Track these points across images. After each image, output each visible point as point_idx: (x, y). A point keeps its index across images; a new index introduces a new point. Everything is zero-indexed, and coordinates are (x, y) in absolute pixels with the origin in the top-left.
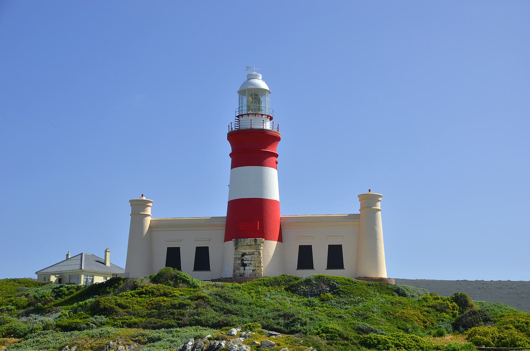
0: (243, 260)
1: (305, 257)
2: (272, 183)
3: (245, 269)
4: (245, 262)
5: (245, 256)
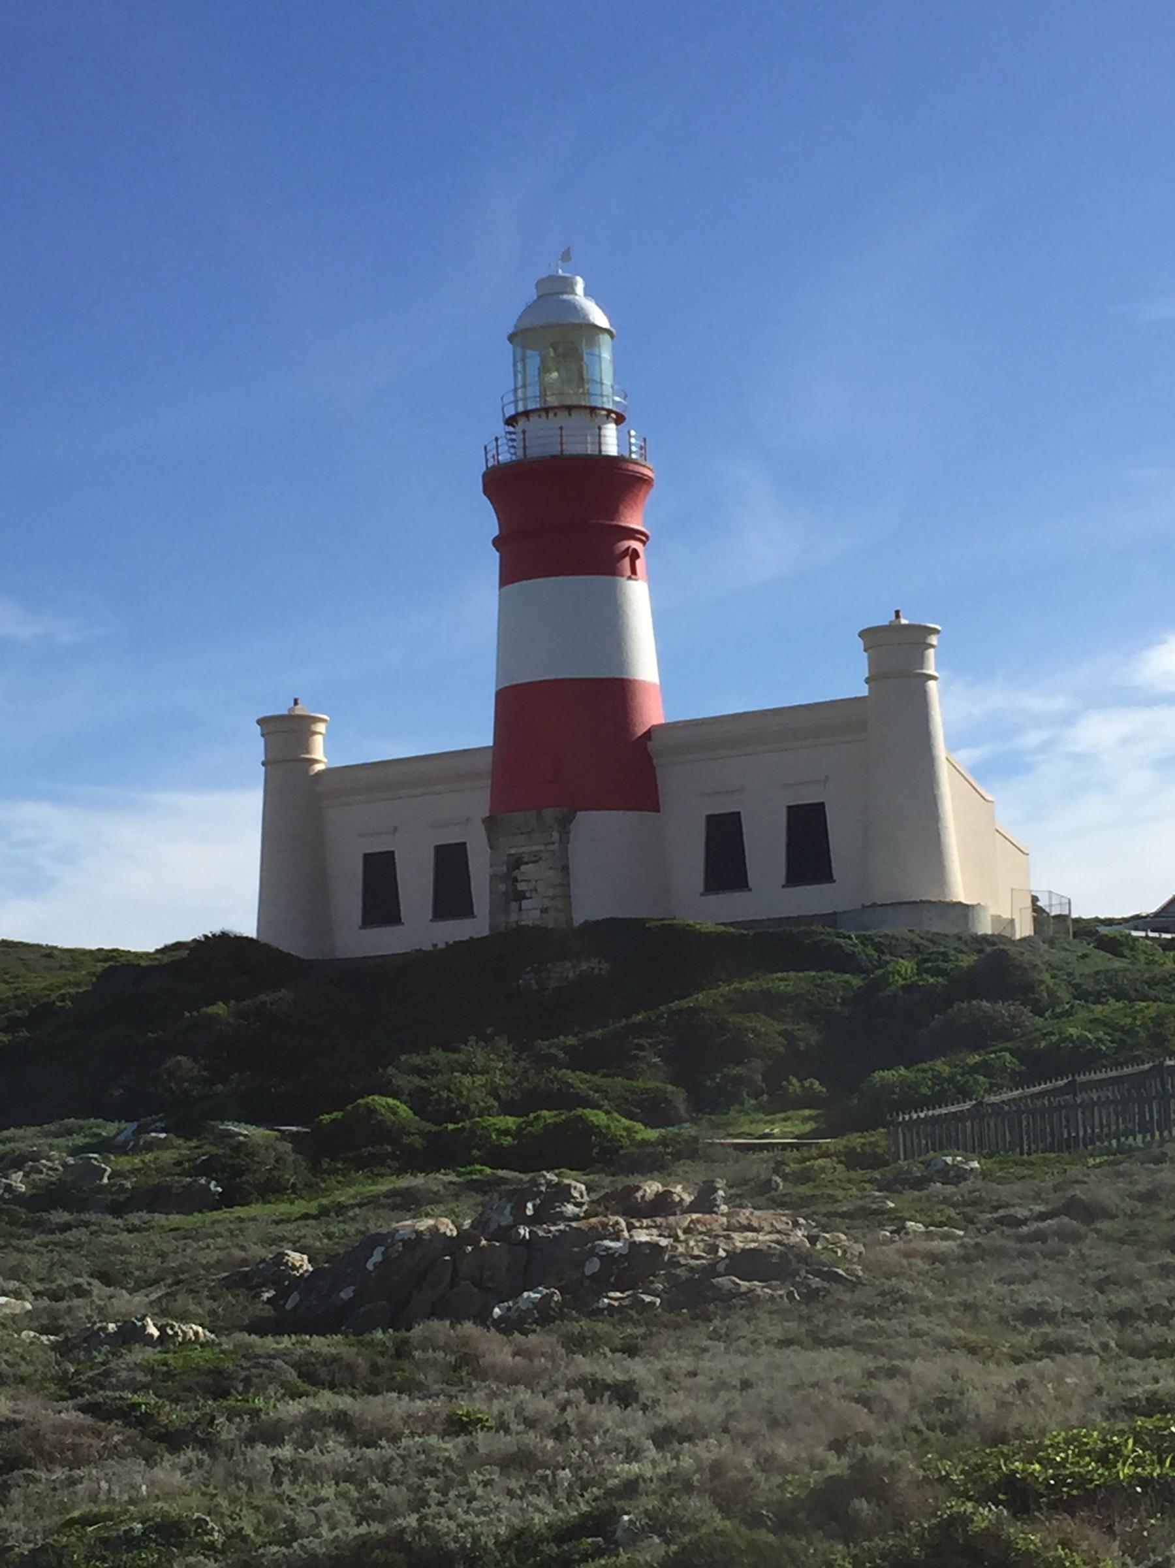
0: (515, 880)
1: (725, 858)
3: (520, 909)
4: (522, 886)
5: (523, 868)
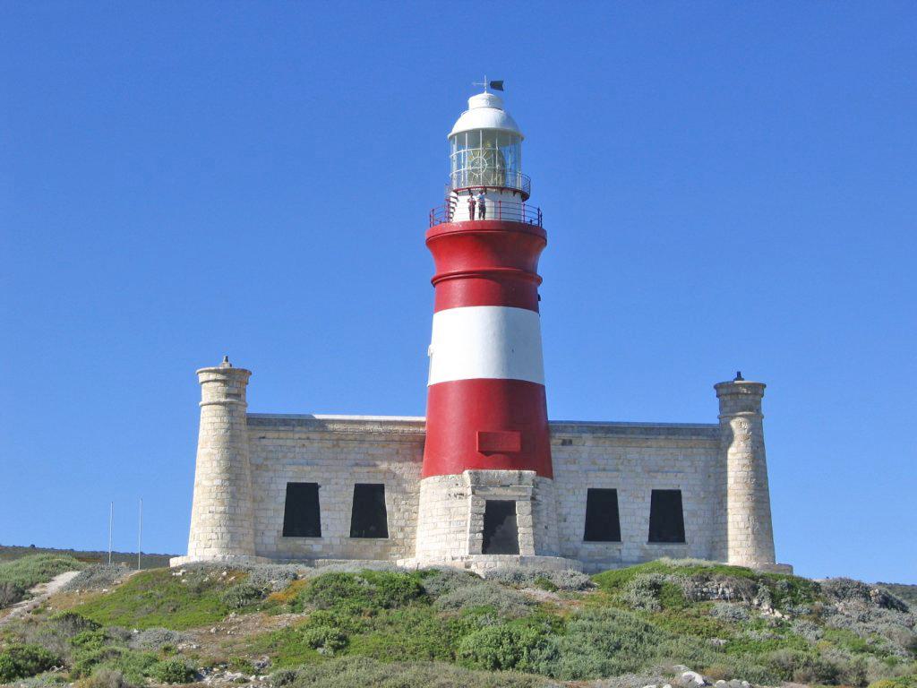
2: (464, 343)
